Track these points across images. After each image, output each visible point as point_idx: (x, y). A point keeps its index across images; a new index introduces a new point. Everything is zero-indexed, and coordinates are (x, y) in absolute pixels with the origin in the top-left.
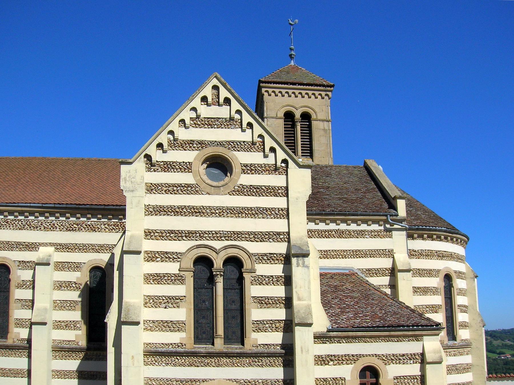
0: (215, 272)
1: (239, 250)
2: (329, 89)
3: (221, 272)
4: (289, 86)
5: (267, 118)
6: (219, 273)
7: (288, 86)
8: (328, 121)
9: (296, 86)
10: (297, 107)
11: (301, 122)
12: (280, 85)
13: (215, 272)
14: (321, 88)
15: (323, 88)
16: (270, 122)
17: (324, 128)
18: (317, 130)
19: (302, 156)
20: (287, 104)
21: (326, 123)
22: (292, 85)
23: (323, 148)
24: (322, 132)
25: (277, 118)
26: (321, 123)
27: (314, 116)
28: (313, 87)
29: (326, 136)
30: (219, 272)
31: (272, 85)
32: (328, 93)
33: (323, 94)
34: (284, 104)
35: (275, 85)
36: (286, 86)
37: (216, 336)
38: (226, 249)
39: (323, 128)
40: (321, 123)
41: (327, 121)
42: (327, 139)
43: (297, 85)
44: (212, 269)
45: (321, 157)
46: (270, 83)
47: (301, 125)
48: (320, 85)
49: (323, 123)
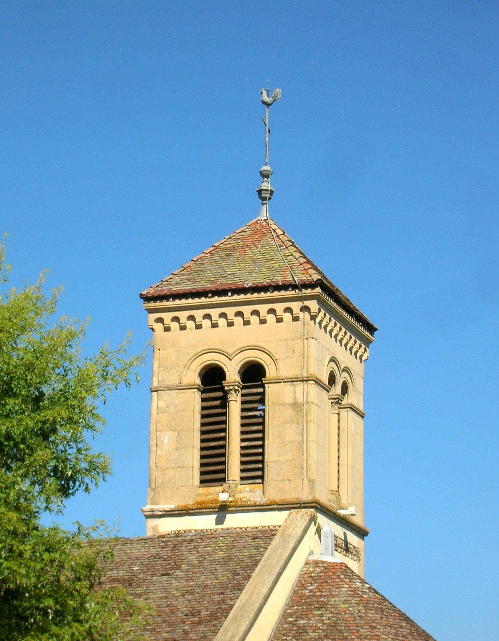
0: (226, 386)
1: (259, 351)
2: (309, 292)
3: (235, 385)
4: (212, 299)
5: (157, 391)
6: (231, 388)
7: (207, 300)
8: (307, 381)
9: (227, 298)
10: (230, 351)
11: (244, 388)
12: (190, 301)
13: (226, 386)
14: (288, 293)
15: (293, 292)
16: (165, 401)
17: (295, 398)
18: (276, 407)
19: (242, 479)
20: (206, 347)
21: (299, 386)
22: (219, 297)
23: (289, 456)
24: (289, 413)
25: (181, 388)
26: (288, 388)
27: (270, 372)
28: (269, 294)
29: (298, 423)
30: (232, 386)
31: (171, 303)
32: (307, 303)
33: (296, 306)
34: (200, 350)
35: (178, 303)
36: (203, 300)
37: (228, 481)
38: (242, 351)
39: (291, 401)
40: (288, 386)
41: (303, 381)
42: (301, 428)
43: (230, 294)
44: (223, 382)
45: (283, 480)
46: (165, 297)
47: (243, 395)
48: (284, 287)
49: (292, 388)
